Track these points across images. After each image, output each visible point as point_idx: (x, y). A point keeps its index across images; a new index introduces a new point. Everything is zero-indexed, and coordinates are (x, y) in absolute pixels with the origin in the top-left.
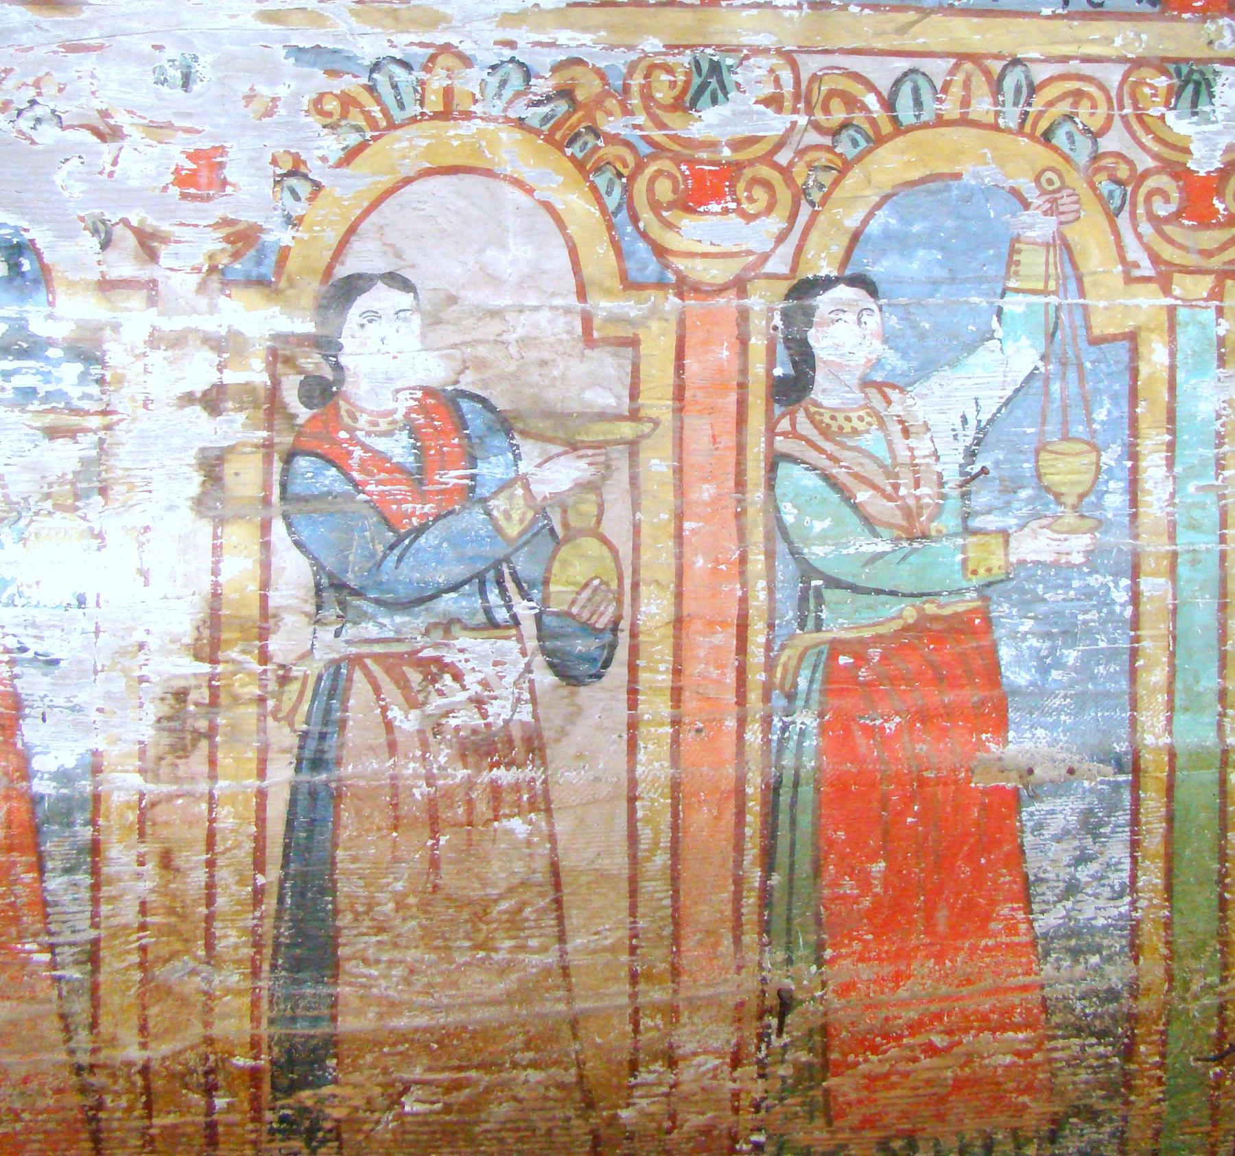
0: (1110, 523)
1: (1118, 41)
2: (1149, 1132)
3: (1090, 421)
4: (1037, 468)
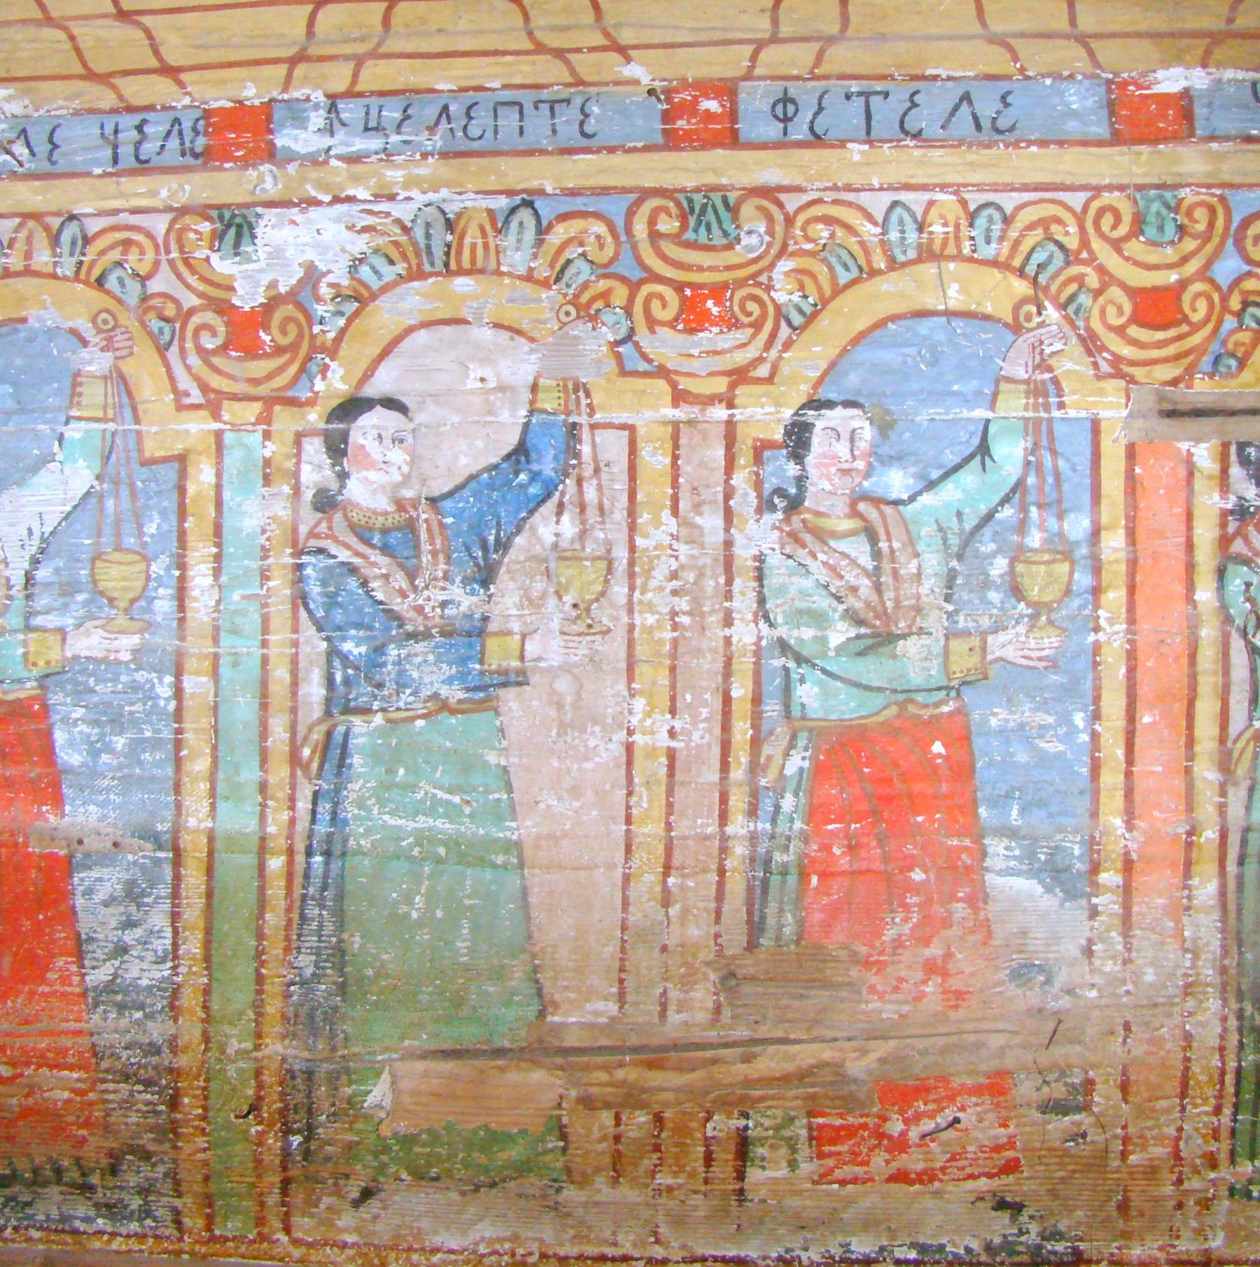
0: (159, 625)
1: (164, 193)
2: (199, 1177)
3: (141, 534)
4: (93, 575)
